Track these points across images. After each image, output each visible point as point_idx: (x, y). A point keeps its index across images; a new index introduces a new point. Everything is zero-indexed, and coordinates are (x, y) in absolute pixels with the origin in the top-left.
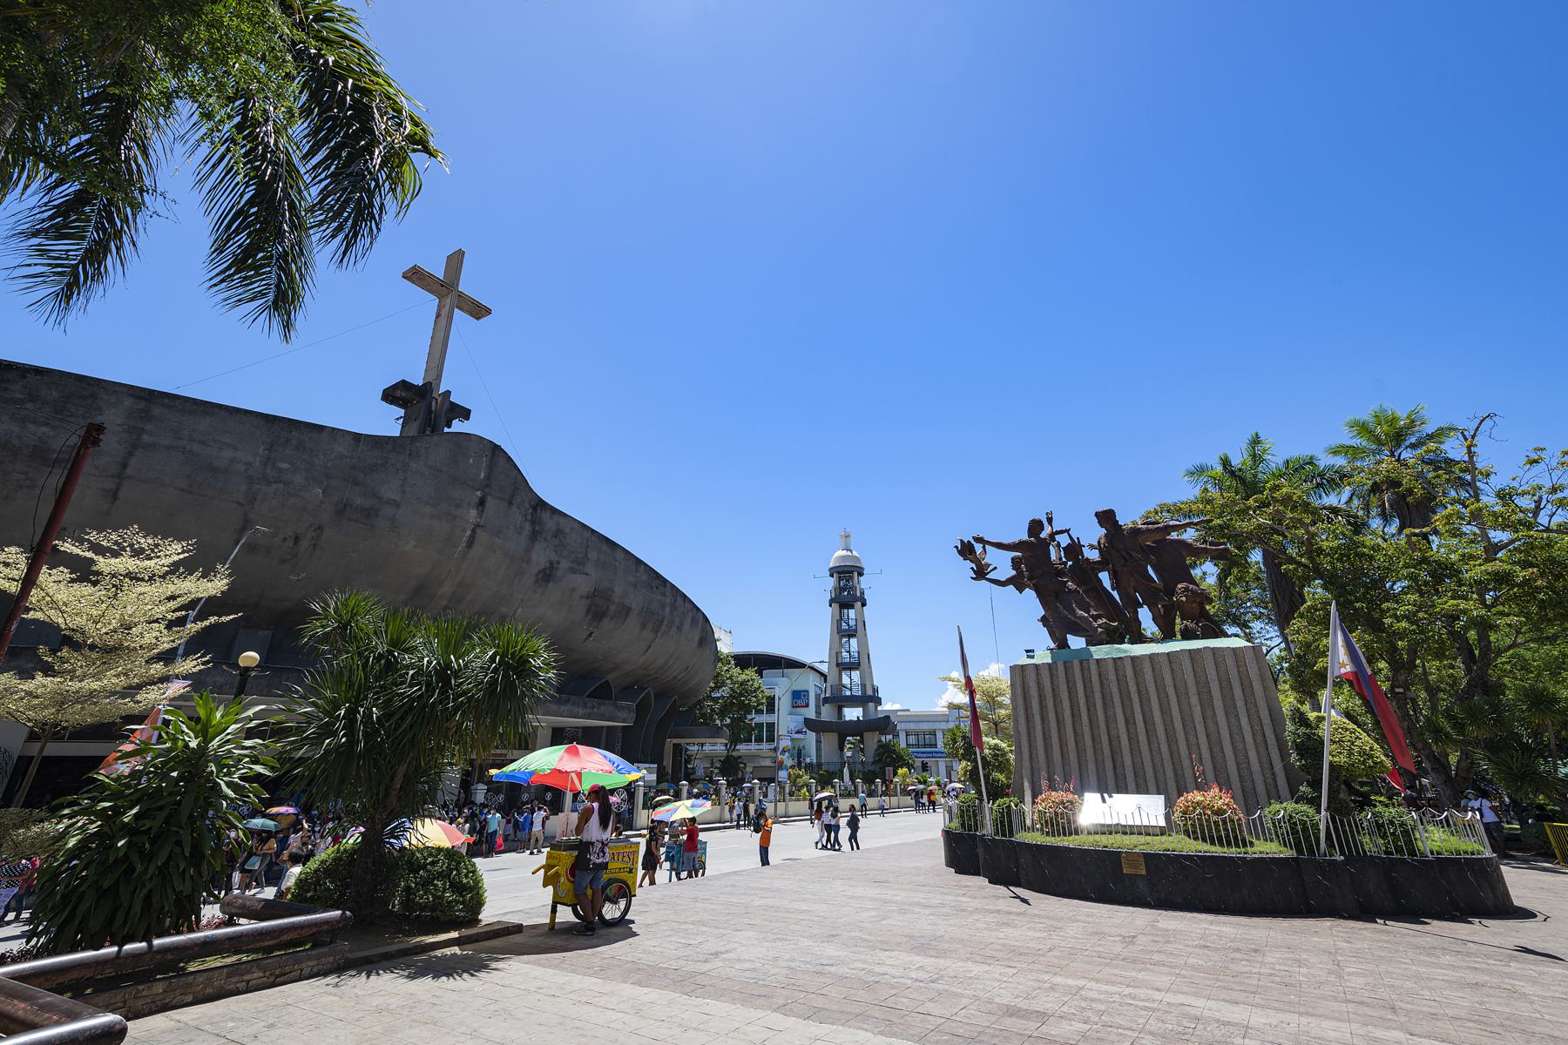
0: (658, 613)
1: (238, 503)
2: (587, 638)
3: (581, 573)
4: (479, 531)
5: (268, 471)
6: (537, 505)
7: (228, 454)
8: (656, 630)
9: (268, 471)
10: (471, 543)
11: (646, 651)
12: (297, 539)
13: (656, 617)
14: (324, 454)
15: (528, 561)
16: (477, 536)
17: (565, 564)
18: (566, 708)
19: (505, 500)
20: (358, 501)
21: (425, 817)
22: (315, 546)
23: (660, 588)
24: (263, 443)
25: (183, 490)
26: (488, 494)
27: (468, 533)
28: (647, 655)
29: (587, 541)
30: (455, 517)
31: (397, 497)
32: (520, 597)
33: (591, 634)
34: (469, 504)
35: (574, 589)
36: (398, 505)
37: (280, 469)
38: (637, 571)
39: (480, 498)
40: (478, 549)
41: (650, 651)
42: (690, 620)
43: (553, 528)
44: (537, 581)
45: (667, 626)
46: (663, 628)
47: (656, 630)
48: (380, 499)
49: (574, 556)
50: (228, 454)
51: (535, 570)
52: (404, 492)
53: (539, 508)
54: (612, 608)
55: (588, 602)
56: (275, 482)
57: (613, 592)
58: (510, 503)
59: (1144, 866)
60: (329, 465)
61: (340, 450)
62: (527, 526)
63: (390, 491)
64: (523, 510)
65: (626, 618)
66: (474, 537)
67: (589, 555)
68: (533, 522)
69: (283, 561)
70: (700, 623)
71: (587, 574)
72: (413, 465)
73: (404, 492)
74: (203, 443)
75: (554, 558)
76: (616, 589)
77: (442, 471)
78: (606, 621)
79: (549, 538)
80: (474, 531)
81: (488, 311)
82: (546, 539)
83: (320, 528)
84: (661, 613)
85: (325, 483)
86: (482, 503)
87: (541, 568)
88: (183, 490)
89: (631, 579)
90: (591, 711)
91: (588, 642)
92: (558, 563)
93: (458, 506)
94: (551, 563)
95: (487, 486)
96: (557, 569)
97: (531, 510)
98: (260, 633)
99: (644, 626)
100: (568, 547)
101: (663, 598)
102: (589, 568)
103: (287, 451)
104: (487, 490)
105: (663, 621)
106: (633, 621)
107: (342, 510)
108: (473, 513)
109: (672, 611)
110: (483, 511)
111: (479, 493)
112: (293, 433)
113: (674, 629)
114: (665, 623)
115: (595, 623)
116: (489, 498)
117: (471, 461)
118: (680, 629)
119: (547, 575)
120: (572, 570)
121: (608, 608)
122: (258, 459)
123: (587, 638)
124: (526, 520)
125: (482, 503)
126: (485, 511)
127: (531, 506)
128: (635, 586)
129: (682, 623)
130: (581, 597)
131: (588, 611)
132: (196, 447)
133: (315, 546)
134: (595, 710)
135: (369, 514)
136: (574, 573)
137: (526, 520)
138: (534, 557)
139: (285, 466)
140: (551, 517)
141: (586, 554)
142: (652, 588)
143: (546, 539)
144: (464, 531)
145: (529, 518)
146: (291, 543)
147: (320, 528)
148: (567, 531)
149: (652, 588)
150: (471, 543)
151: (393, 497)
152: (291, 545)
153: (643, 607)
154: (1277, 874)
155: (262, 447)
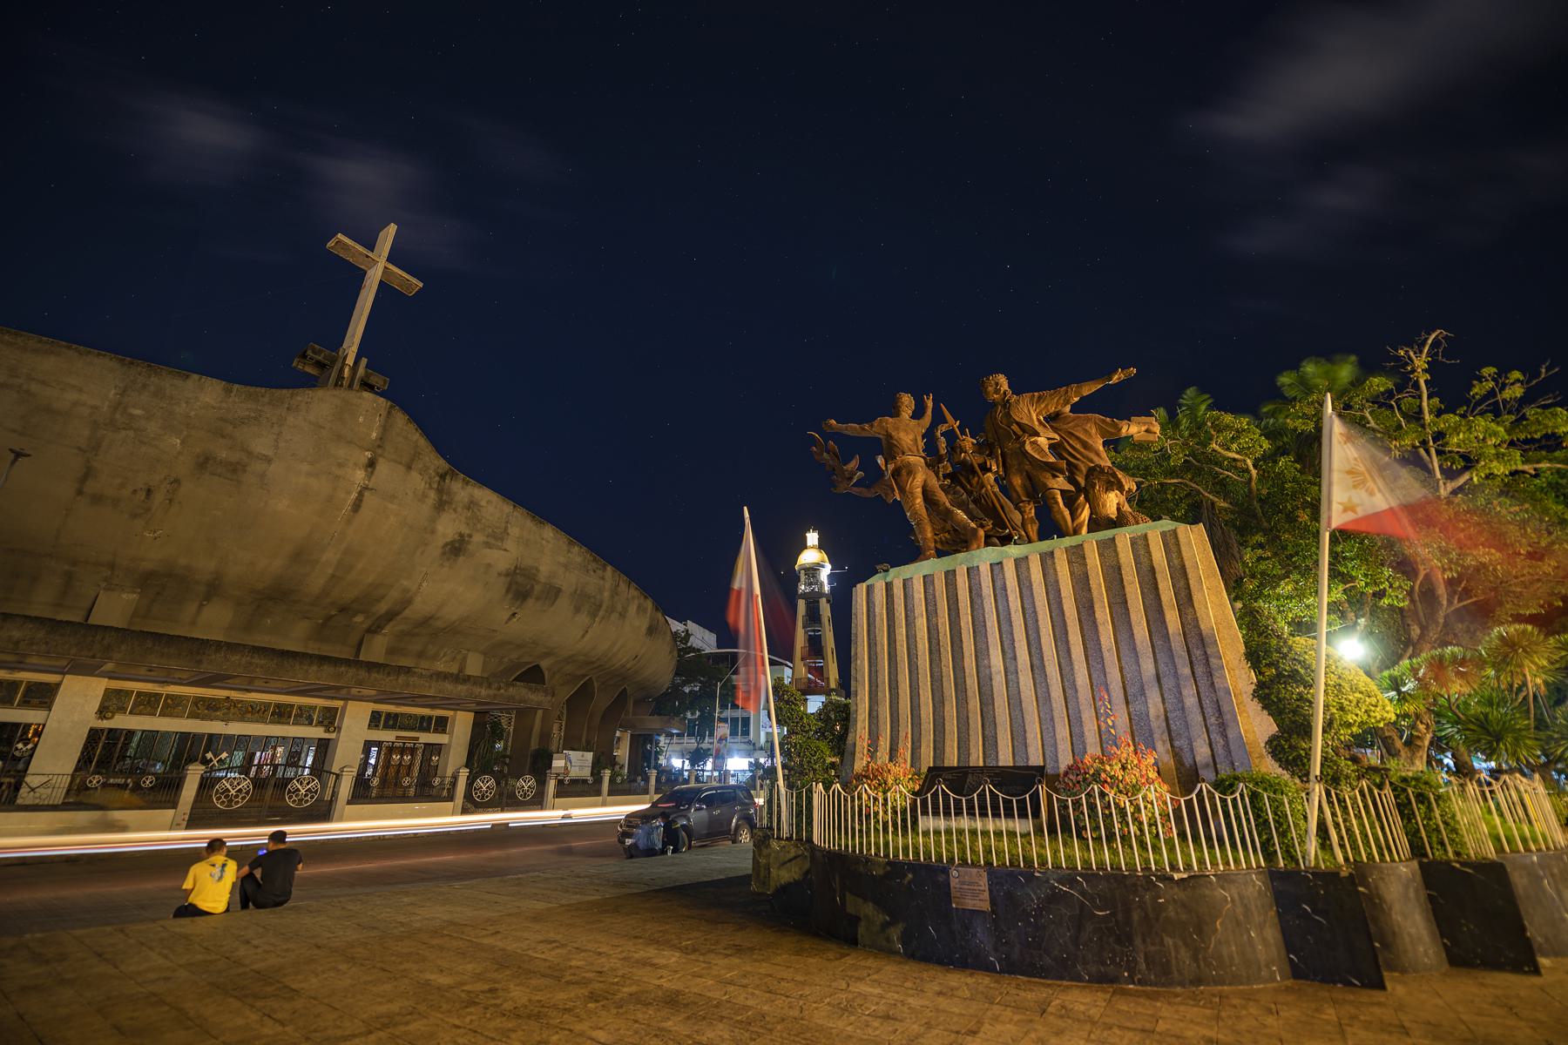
0: (594, 597)
1: (80, 449)
2: (509, 619)
3: (499, 548)
4: (367, 494)
5: (118, 416)
6: (446, 474)
7: (71, 396)
8: (593, 615)
9: (118, 416)
10: (357, 506)
11: (583, 636)
12: (149, 491)
13: (592, 600)
14: (187, 403)
15: (433, 532)
16: (365, 499)
17: (478, 538)
18: (465, 687)
19: (401, 463)
20: (224, 454)
21: (1107, 877)
22: (170, 501)
23: (598, 571)
24: (115, 387)
25: (14, 431)
26: (380, 456)
27: (354, 495)
28: (585, 639)
29: (508, 516)
30: (337, 477)
31: (270, 453)
32: (425, 569)
33: (514, 614)
34: (355, 464)
35: (489, 565)
36: (269, 460)
37: (131, 415)
38: (569, 551)
39: (369, 459)
40: (366, 512)
41: (588, 636)
42: (635, 607)
43: (466, 500)
44: (444, 554)
45: (606, 611)
46: (601, 613)
47: (593, 615)
48: (250, 454)
49: (490, 530)
50: (71, 396)
51: (441, 542)
52: (277, 447)
53: (448, 478)
54: (538, 588)
55: (509, 579)
56: (124, 429)
57: (538, 570)
58: (409, 468)
59: (986, 895)
60: (192, 413)
61: (207, 399)
62: (432, 495)
63: (261, 445)
64: (426, 478)
65: (555, 601)
66: (361, 501)
67: (509, 531)
68: (440, 491)
69: (134, 516)
70: (649, 610)
71: (505, 550)
72: (291, 419)
73: (277, 447)
74: (44, 383)
75: (466, 531)
76: (542, 568)
77: (324, 428)
78: (531, 601)
79: (459, 509)
80: (361, 494)
81: (1523, 959)
82: (455, 510)
83: (177, 481)
84: (598, 597)
85: (185, 433)
86: (371, 464)
87: (448, 540)
88: (14, 431)
89: (562, 559)
90: (496, 692)
91: (511, 622)
92: (470, 536)
93: (340, 465)
94: (461, 535)
95: (379, 446)
96: (469, 543)
97: (437, 479)
98: (124, 596)
99: (578, 610)
100: (483, 521)
101: (602, 582)
102: (509, 544)
103: (142, 397)
104: (379, 451)
105: (600, 606)
106: (564, 603)
107: (204, 463)
108: (360, 475)
109: (612, 596)
110: (372, 473)
111: (368, 454)
112: (152, 379)
113: (615, 616)
114: (604, 607)
115: (518, 603)
116: (381, 460)
117: (361, 419)
118: (623, 615)
119: (456, 548)
120: (488, 545)
121: (532, 587)
122: (107, 403)
123: (509, 619)
124: (431, 488)
125: (371, 464)
126: (376, 472)
127: (437, 473)
128: (566, 566)
129: (625, 610)
130: (499, 574)
131: (508, 590)
132: (34, 387)
133: (170, 501)
134: (502, 691)
135: (235, 469)
136: (490, 548)
137: (431, 488)
138: (440, 528)
139: (137, 412)
140: (463, 488)
141: (506, 528)
142: (587, 571)
143: (455, 510)
144: (349, 493)
145: (435, 486)
146: (142, 495)
147: (177, 481)
148: (483, 503)
149: (587, 571)
150: (357, 506)
151: (264, 452)
152: (143, 498)
153: (576, 590)
154: (1229, 905)
155: (113, 392)
